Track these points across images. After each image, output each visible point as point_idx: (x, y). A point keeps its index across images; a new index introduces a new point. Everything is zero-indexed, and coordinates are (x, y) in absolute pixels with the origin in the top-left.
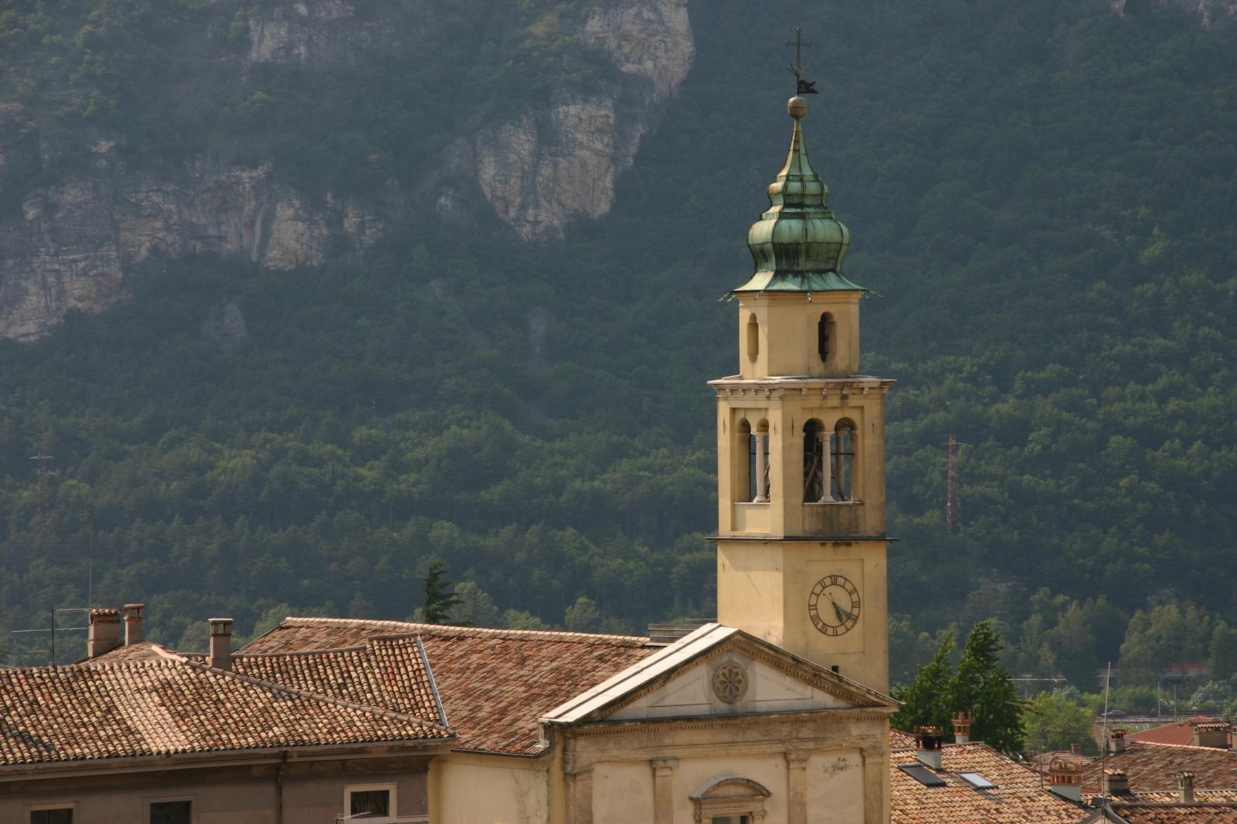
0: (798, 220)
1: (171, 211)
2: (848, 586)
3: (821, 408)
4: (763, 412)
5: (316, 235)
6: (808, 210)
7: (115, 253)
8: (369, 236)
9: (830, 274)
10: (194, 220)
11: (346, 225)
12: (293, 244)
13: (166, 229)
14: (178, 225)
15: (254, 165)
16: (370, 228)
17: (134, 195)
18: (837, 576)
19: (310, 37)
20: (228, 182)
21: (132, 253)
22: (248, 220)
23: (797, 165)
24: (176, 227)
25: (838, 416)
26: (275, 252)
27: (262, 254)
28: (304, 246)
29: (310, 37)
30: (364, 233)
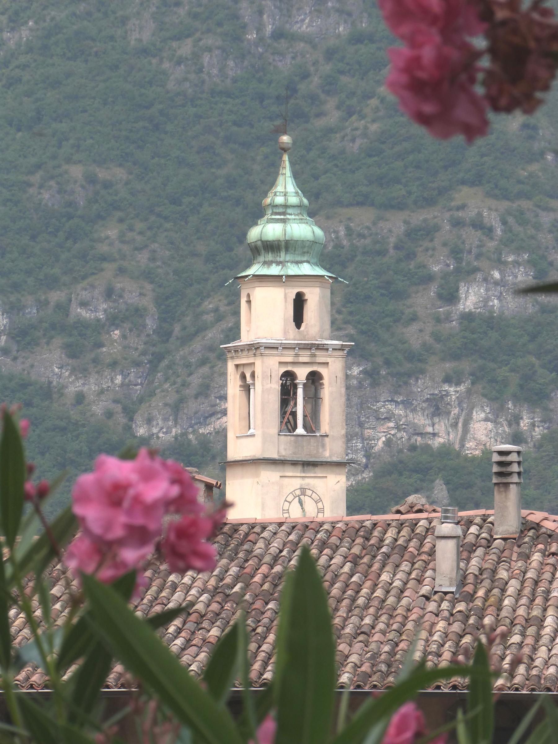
0: (281, 224)
1: (401, 415)
2: (314, 496)
3: (294, 363)
4: (253, 366)
5: (500, 432)
6: (288, 217)
7: (361, 445)
8: (538, 432)
9: (305, 264)
10: (416, 421)
11: (522, 425)
12: (484, 438)
13: (397, 428)
14: (405, 425)
15: (458, 384)
16: (538, 427)
17: (375, 404)
18: (306, 489)
19: (501, 293)
20: (440, 394)
21: (373, 445)
22: (453, 421)
23: (284, 184)
24: (404, 426)
25: (309, 369)
26: (471, 444)
27: (462, 446)
28: (492, 440)
29: (501, 293)
30: (534, 430)
